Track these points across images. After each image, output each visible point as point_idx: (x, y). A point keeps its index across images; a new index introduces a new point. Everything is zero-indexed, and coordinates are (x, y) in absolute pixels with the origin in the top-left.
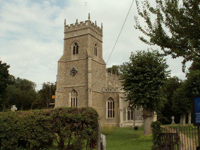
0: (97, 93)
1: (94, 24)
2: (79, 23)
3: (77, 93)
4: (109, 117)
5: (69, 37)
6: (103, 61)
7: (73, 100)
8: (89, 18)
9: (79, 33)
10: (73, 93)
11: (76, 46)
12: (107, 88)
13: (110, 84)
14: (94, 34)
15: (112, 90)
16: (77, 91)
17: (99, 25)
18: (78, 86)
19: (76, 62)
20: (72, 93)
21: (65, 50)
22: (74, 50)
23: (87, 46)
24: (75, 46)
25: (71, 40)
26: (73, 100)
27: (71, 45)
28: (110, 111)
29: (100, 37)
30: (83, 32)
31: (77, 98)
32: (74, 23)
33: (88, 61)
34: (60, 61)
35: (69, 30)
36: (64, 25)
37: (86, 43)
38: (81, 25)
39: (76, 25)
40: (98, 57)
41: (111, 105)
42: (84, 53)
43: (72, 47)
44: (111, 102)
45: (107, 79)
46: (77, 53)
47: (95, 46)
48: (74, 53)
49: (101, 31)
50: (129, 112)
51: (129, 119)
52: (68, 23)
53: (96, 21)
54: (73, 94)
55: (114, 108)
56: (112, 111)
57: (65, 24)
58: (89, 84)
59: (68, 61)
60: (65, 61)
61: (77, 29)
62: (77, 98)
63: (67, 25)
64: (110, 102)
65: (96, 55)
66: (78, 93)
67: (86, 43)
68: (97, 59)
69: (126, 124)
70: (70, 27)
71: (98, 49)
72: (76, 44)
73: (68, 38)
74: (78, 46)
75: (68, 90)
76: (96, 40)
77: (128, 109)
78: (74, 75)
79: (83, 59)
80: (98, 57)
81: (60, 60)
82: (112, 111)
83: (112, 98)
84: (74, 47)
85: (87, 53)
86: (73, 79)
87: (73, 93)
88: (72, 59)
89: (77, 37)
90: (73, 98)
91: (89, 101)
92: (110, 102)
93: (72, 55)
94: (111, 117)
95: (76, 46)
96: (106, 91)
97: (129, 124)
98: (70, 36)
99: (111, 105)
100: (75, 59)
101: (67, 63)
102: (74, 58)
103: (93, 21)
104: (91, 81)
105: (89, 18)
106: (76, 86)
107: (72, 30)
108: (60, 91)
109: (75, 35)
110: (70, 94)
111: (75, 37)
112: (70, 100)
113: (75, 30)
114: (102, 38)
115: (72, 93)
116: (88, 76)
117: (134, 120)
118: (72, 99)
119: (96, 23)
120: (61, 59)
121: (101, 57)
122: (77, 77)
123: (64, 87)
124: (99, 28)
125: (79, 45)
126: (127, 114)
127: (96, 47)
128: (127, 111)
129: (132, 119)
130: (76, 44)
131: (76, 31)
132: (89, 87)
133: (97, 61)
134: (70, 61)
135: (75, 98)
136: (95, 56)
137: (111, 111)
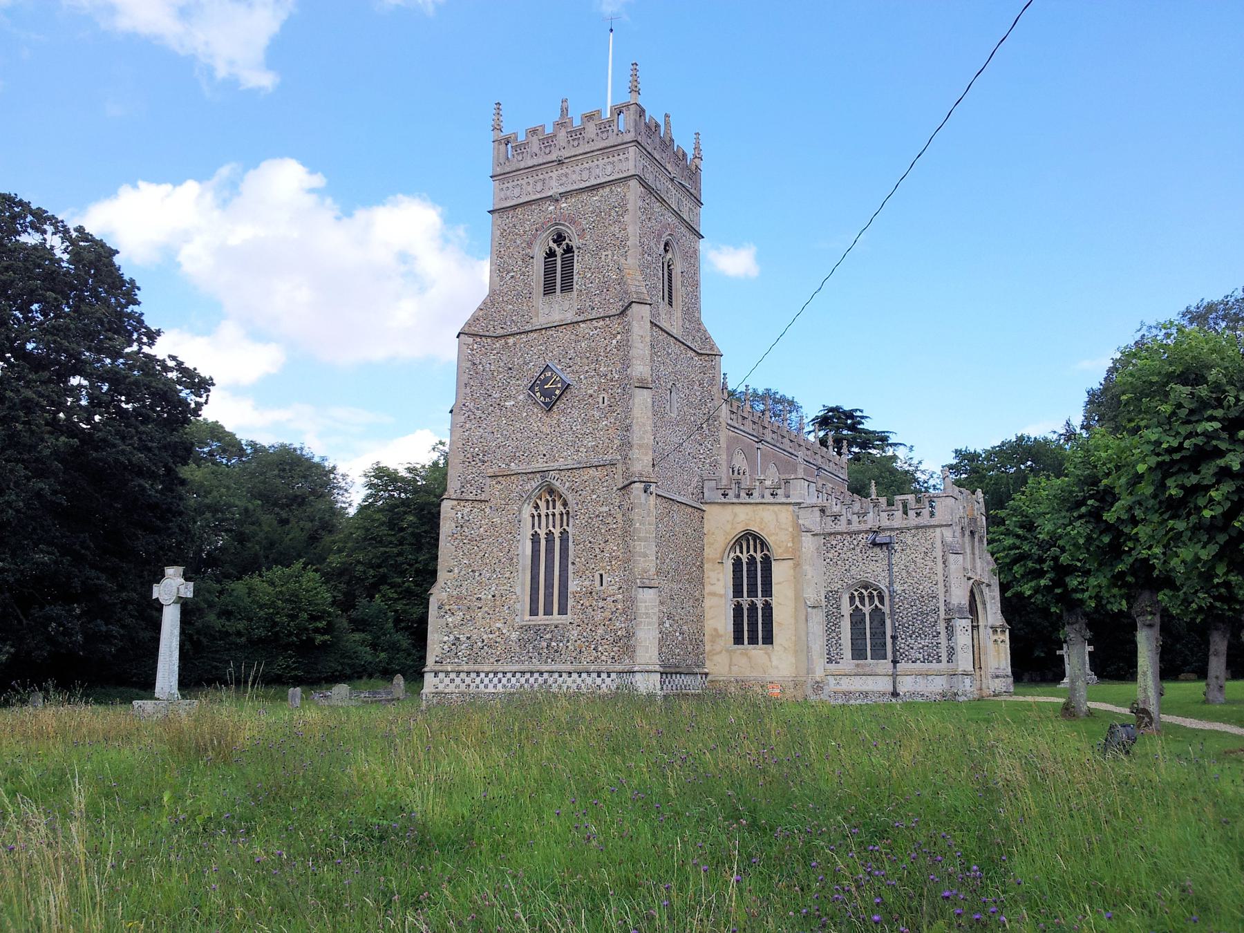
0: (675, 507)
1: (657, 126)
2: (577, 123)
3: (565, 504)
4: (534, 612)
5: (521, 201)
6: (706, 339)
7: (543, 542)
8: (635, 90)
9: (576, 177)
10: (542, 504)
11: (559, 251)
12: (724, 482)
13: (740, 462)
14: (662, 185)
15: (756, 494)
16: (570, 498)
17: (683, 142)
18: (570, 463)
19: (565, 335)
20: (537, 507)
21: (500, 270)
22: (549, 272)
23: (622, 243)
24: (554, 246)
25: (534, 217)
26: (543, 542)
27: (530, 245)
28: (745, 607)
29: (687, 204)
30: (602, 170)
31: (564, 533)
32: (548, 119)
33: (629, 323)
34: (474, 330)
35: (415, 675)
36: (492, 136)
37: (615, 229)
38: (591, 129)
39: (562, 134)
40: (678, 313)
41: (550, 550)
42: (605, 286)
43: (539, 253)
44: (752, 561)
45: (724, 435)
46: (567, 287)
47: (666, 251)
48: (549, 289)
49: (694, 174)
50: (857, 619)
51: (858, 653)
52: (516, 126)
53: (667, 116)
54: (543, 511)
55: (768, 591)
56: (760, 606)
57: (497, 128)
58: (635, 453)
59: (515, 329)
60: (500, 332)
61: (566, 153)
62: (564, 533)
63: (507, 131)
64: (745, 560)
65: (670, 304)
66: (572, 505)
67: (615, 229)
68: (674, 322)
69: (847, 684)
70: (524, 145)
71: (677, 269)
72: (559, 239)
73: (514, 207)
74: (569, 250)
75: (516, 486)
76: (672, 219)
77: (852, 598)
78: (549, 407)
79: (603, 318)
80: (678, 313)
81: (468, 324)
82: (760, 606)
83: (756, 537)
84: (551, 254)
85: (621, 282)
86: (546, 430)
87: (542, 504)
88: (540, 321)
89: (565, 195)
90: (542, 533)
91: (640, 547)
92: (745, 560)
93: (539, 300)
94: (548, 612)
95: (559, 251)
96: (725, 495)
97: (857, 684)
98: (528, 190)
99: (550, 550)
100: (556, 317)
101: (511, 341)
102: (559, 309)
103: (654, 113)
104: (649, 439)
105: (635, 90)
106: (561, 463)
107: (535, 161)
108: (471, 497)
109: (555, 189)
110: (528, 510)
111: (554, 200)
112: (529, 544)
113: (553, 157)
114: (698, 215)
115: (537, 507)
116: (628, 411)
117: (895, 662)
118: (535, 539)
119: (667, 124)
120: (475, 319)
121: (692, 313)
122: (569, 416)
123: (490, 472)
124: (684, 155)
125: (575, 242)
126: (846, 625)
127: (669, 256)
128: (846, 609)
129: (879, 653)
130: (559, 239)
131: (560, 163)
132: (637, 468)
133: (674, 332)
134: (527, 328)
135: (557, 532)
136: (663, 306)
137: (753, 607)
